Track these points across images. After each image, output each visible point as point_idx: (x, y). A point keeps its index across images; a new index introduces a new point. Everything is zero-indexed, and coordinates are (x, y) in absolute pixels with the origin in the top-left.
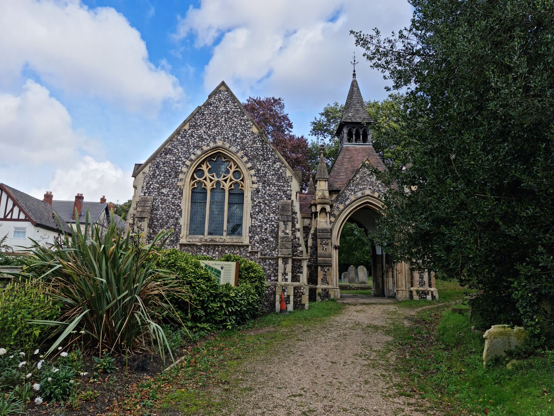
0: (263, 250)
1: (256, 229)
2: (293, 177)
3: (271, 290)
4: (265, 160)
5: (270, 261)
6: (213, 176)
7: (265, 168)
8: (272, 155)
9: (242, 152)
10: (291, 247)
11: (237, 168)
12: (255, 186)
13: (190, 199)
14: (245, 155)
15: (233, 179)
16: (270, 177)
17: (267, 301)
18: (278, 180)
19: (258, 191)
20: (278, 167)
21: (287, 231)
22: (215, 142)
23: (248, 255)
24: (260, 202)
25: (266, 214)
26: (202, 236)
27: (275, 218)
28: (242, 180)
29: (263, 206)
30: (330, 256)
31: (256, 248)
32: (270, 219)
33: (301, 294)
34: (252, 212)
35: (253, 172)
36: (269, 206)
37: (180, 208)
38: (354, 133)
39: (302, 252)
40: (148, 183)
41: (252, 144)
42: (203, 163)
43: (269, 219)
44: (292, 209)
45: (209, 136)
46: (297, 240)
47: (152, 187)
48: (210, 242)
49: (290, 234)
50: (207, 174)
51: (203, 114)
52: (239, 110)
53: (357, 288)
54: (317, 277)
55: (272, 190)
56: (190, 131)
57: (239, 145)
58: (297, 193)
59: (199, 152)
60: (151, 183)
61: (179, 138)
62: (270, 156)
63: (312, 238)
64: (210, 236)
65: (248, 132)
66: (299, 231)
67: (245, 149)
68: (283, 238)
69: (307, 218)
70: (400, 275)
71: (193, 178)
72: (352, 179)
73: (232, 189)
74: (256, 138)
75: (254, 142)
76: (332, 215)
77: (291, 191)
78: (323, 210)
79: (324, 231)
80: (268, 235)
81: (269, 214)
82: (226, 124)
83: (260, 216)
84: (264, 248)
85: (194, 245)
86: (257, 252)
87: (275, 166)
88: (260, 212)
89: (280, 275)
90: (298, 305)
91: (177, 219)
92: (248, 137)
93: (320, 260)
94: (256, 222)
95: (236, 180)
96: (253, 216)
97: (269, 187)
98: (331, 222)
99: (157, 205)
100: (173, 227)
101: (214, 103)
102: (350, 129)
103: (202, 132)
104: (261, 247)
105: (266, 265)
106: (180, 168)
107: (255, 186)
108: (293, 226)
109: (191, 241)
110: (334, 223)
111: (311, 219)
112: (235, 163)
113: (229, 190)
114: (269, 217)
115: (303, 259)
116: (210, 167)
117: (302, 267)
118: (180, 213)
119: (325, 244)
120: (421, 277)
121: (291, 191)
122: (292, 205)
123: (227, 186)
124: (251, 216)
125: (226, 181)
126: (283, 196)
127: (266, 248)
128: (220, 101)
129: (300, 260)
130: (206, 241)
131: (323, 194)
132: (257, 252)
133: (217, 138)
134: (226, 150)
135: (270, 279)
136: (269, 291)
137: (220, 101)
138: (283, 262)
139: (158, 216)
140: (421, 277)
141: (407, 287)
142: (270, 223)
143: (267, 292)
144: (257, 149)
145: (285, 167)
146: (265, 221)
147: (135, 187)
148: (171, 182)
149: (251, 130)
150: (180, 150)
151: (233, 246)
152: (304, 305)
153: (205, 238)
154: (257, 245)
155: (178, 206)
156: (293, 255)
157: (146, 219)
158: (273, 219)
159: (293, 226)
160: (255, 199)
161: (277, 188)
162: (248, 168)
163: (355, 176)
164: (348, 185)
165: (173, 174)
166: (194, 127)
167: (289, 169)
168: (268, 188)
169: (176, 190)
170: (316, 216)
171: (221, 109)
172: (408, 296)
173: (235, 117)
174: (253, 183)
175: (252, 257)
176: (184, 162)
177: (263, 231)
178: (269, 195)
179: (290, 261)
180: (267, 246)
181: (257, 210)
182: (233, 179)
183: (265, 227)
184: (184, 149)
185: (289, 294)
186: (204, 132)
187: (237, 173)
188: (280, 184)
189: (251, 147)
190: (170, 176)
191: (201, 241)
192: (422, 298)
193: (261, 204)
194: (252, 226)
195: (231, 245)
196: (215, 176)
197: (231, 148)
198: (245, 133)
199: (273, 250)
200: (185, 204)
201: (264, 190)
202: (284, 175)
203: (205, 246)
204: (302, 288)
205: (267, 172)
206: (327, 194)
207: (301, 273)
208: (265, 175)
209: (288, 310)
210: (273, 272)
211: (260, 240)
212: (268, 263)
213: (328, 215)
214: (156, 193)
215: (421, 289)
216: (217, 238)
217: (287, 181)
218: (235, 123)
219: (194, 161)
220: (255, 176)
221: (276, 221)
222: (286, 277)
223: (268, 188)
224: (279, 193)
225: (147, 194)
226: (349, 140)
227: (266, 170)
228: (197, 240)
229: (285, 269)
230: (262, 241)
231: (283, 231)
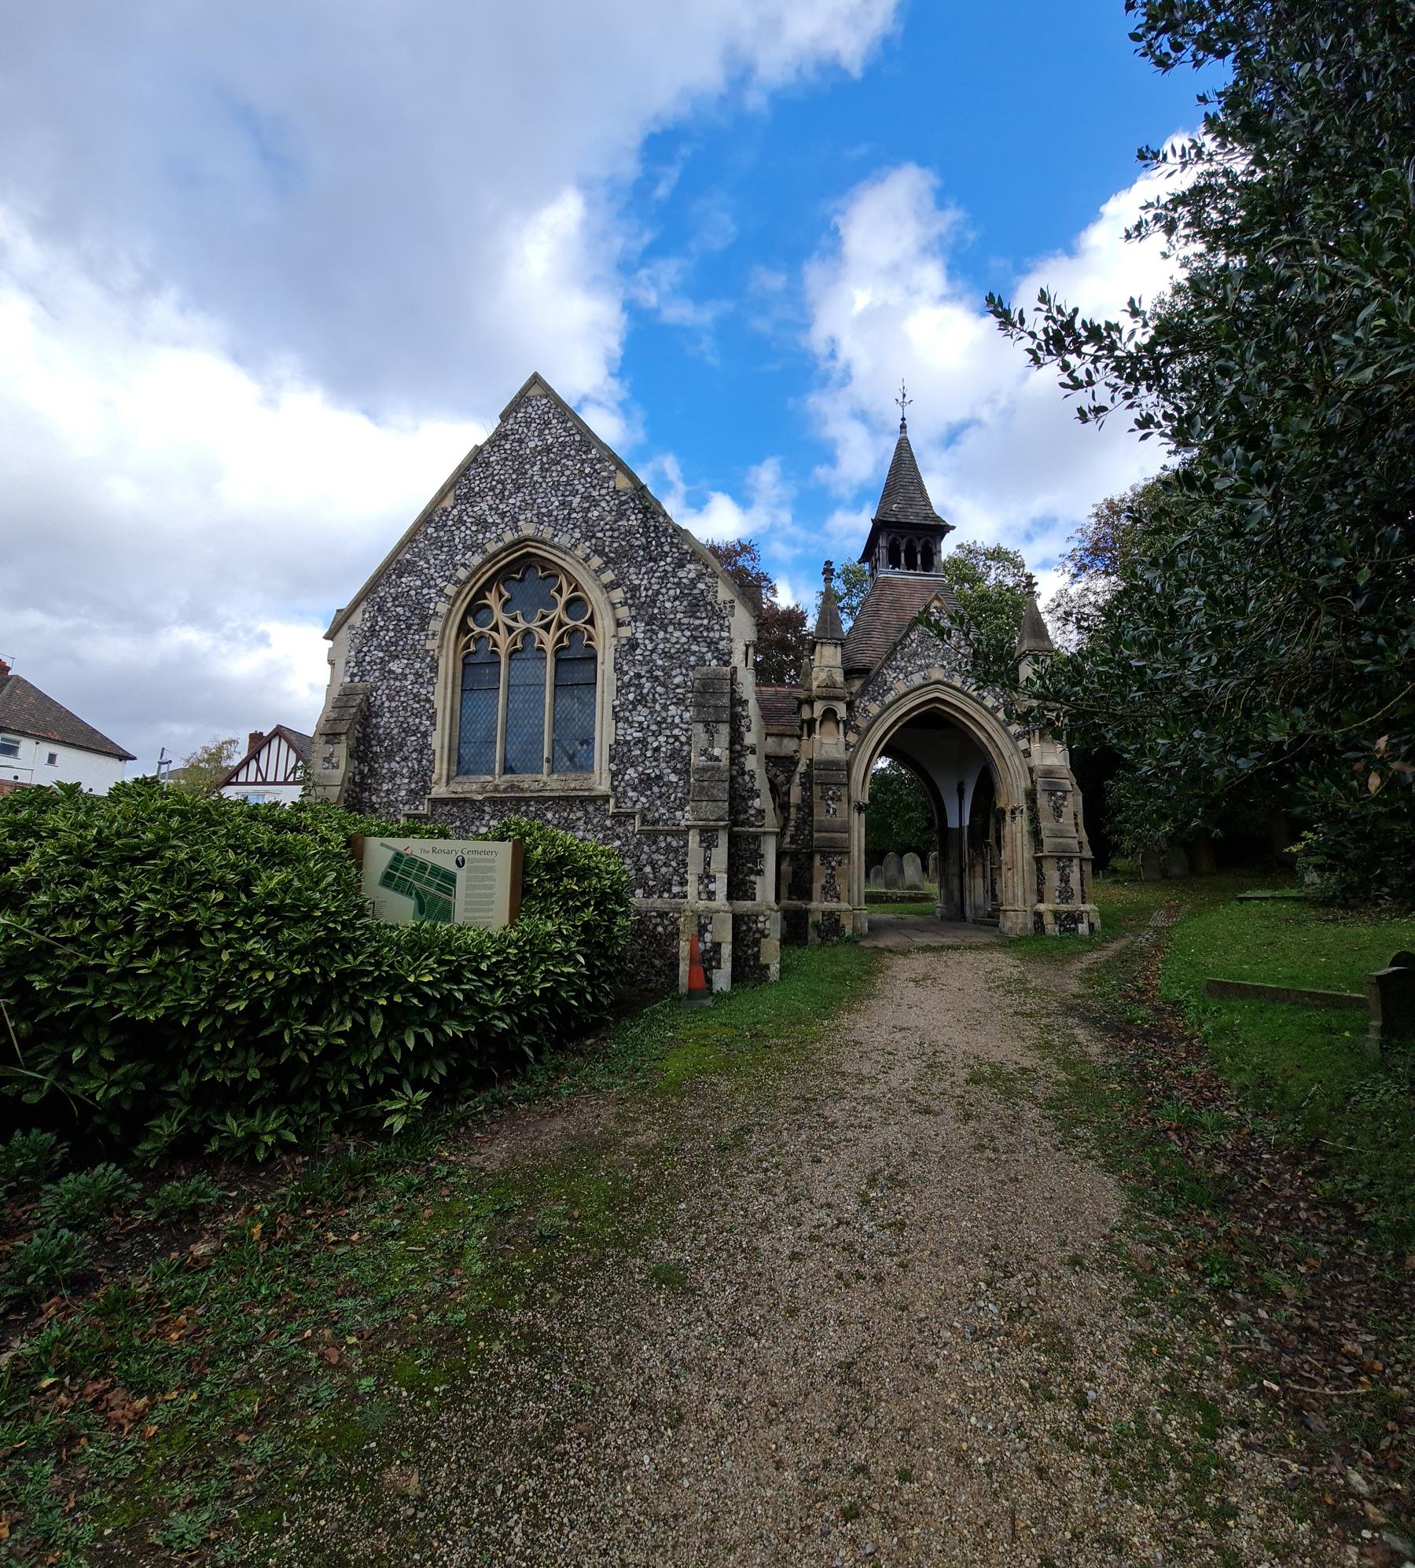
0: (649, 809)
1: (630, 751)
2: (737, 603)
3: (672, 923)
4: (651, 559)
5: (669, 839)
6: (515, 619)
7: (653, 580)
8: (672, 544)
9: (587, 544)
10: (726, 796)
11: (575, 590)
12: (626, 632)
13: (459, 681)
14: (595, 551)
15: (566, 619)
16: (668, 605)
17: (661, 957)
18: (692, 611)
19: (633, 644)
20: (692, 575)
21: (717, 752)
22: (517, 529)
23: (608, 823)
24: (638, 676)
25: (658, 707)
26: (489, 778)
27: (681, 717)
28: (591, 621)
29: (648, 685)
30: (846, 829)
31: (630, 804)
32: (669, 720)
33: (757, 936)
34: (617, 703)
35: (618, 595)
36: (664, 685)
37: (432, 707)
38: (903, 548)
39: (761, 812)
40: (360, 651)
41: (616, 521)
42: (487, 586)
43: (665, 719)
44: (733, 692)
45: (503, 515)
46: (747, 778)
47: (368, 659)
48: (505, 791)
49: (725, 762)
50: (499, 616)
51: (488, 464)
52: (578, 438)
53: (902, 899)
54: (812, 882)
55: (674, 640)
56: (455, 512)
57: (579, 527)
58: (747, 646)
59: (477, 560)
60: (365, 649)
61: (430, 530)
62: (666, 548)
63: (802, 784)
64: (508, 777)
65: (604, 492)
66: (753, 752)
67: (594, 536)
68: (705, 769)
69: (791, 736)
70: (1010, 873)
71: (464, 628)
72: (900, 643)
73: (564, 648)
74: (626, 502)
75: (622, 515)
76: (852, 728)
77: (731, 640)
78: (830, 714)
79: (830, 765)
80: (664, 765)
81: (665, 707)
82: (544, 477)
83: (641, 715)
84: (652, 803)
85: (465, 800)
86: (631, 816)
87: (681, 574)
88: (640, 702)
89: (691, 878)
90: (747, 970)
91: (425, 735)
92: (603, 504)
93: (818, 839)
94: (629, 731)
95: (572, 623)
96: (621, 714)
97: (666, 632)
98: (848, 746)
99: (378, 703)
100: (414, 755)
101: (514, 432)
102: (894, 540)
103: (485, 507)
104: (643, 799)
105: (657, 851)
106: (432, 606)
107: (626, 632)
108: (736, 737)
109: (460, 790)
110: (857, 747)
111: (800, 737)
112: (570, 579)
113: (557, 652)
114: (664, 714)
115: (765, 833)
116: (507, 595)
117: (762, 856)
118: (432, 718)
119: (832, 799)
120: (1065, 879)
121: (731, 640)
122: (733, 681)
123: (549, 640)
124: (615, 714)
125: (546, 627)
126: (709, 656)
127: (658, 802)
128: (528, 426)
129: (756, 837)
130: (496, 789)
131: (830, 676)
132: (631, 816)
133: (522, 517)
134: (545, 543)
135: (669, 891)
136: (665, 928)
137: (528, 426)
138: (701, 841)
139: (381, 731)
140: (1065, 879)
141: (1029, 903)
142: (668, 732)
143: (660, 929)
144: (629, 532)
145: (714, 575)
146: (654, 727)
147: (331, 662)
148: (410, 642)
149: (611, 483)
150: (432, 561)
151: (567, 798)
152: (767, 967)
153: (497, 782)
154: (631, 794)
155: (428, 700)
156: (735, 823)
157: (343, 737)
158: (677, 720)
159: (736, 737)
160: (626, 668)
161: (688, 633)
162: (605, 586)
163: (907, 635)
164: (891, 656)
165: (417, 621)
166: (468, 498)
167: (725, 582)
168: (661, 635)
169: (423, 660)
170: (811, 731)
171: (532, 444)
172: (1030, 925)
173: (567, 456)
174: (619, 624)
175: (620, 830)
176: (442, 590)
177: (649, 754)
178: (666, 655)
179: (723, 839)
180: (660, 798)
181: (631, 697)
182: (566, 619)
183: (655, 744)
184: (443, 557)
185: (717, 940)
186: (491, 509)
187: (576, 604)
188: (697, 622)
189: (612, 529)
190: (409, 627)
191: (484, 790)
192: (1067, 930)
193: (644, 680)
194: (617, 742)
195: (559, 797)
196: (520, 618)
197: (556, 539)
198: (595, 493)
199: (676, 810)
200: (442, 696)
201: (651, 640)
202: (710, 598)
203: (493, 801)
204: (761, 918)
205: (658, 593)
206: (839, 677)
207: (760, 873)
208: (654, 601)
209: (716, 987)
210: (676, 871)
211: (641, 781)
212: (663, 845)
213: (841, 726)
214: (377, 674)
215: (1064, 907)
216: (526, 780)
217: (718, 615)
218: (567, 473)
219: (465, 583)
220: (624, 604)
221: (685, 726)
222: (712, 887)
223: (661, 635)
224: (694, 648)
225: (357, 679)
226: (894, 562)
227: (656, 587)
228: (474, 787)
229: (709, 864)
230: (646, 782)
231: (704, 752)
